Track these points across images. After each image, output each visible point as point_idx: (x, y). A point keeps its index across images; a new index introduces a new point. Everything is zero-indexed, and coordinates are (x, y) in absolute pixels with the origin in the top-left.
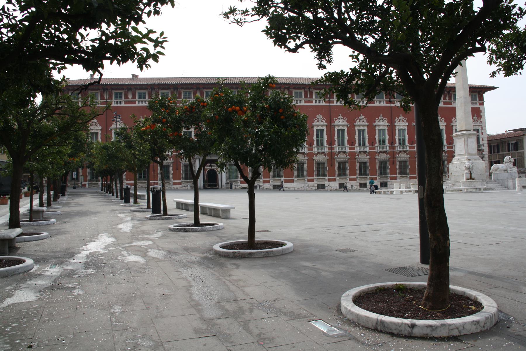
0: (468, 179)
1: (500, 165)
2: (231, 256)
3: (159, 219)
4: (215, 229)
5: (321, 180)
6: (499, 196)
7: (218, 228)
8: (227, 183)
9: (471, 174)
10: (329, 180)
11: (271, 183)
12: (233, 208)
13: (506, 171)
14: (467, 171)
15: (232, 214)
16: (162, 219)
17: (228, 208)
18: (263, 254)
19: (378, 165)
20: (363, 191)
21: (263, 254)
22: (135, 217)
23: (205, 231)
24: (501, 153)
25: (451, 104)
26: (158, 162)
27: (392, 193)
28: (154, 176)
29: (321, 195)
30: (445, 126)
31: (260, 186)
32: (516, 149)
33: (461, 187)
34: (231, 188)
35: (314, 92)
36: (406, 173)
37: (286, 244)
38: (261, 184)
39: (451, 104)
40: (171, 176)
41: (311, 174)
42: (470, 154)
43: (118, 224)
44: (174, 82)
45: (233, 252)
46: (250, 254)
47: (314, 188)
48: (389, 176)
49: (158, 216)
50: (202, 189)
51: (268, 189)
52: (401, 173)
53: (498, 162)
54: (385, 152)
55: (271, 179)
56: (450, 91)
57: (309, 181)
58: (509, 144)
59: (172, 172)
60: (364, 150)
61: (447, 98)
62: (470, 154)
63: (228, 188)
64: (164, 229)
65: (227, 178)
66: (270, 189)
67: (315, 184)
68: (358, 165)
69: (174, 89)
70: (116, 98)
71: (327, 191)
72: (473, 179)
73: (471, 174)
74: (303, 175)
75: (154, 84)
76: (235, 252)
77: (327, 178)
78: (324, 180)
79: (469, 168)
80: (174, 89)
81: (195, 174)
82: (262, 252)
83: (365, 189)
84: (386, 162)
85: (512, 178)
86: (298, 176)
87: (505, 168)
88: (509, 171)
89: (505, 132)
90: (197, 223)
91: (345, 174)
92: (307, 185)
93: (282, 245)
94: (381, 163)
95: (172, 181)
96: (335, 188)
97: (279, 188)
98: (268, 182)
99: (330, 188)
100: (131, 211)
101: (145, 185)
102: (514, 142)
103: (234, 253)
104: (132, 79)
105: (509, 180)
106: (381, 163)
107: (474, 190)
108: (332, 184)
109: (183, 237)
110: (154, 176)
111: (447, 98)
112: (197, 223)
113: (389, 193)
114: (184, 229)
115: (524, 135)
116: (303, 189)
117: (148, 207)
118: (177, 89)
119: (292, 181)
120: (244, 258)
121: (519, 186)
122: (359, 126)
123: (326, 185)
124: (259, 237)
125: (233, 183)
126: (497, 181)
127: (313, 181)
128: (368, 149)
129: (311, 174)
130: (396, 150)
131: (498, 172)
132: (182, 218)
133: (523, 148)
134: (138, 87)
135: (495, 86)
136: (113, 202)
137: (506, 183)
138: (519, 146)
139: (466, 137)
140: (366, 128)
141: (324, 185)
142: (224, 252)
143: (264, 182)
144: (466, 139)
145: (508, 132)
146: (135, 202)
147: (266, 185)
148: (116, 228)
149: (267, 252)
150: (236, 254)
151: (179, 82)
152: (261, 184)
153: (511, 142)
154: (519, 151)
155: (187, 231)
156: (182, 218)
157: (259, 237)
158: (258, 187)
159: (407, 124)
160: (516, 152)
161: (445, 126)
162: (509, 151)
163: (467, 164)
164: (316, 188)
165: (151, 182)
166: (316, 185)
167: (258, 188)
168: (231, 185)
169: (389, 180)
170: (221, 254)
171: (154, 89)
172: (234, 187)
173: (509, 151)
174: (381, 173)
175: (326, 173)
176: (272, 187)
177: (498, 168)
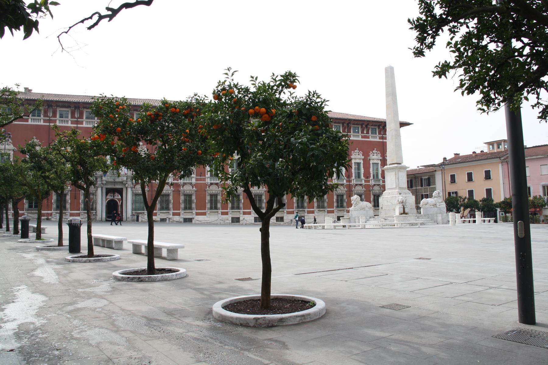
0: (401, 214)
1: (429, 200)
2: (252, 325)
3: (85, 262)
4: (178, 277)
5: (235, 213)
6: (432, 231)
7: (182, 276)
8: (133, 215)
9: (404, 208)
10: (244, 213)
11: (182, 216)
12: (183, 247)
13: (435, 205)
14: (401, 205)
15: (181, 254)
16: (90, 261)
17: (176, 247)
18: (298, 319)
19: (182, 198)
20: (280, 225)
21: (298, 319)
22: (49, 258)
23: (166, 280)
24: (414, 188)
25: (369, 138)
26: (83, 188)
27: (323, 228)
28: (48, 205)
29: (235, 230)
30: (363, 159)
31: (169, 219)
32: (429, 185)
33: (395, 222)
34: (138, 220)
35: (58, 110)
36: (323, 207)
37: (314, 305)
38: (171, 216)
39: (369, 138)
40: (68, 206)
41: (177, 207)
42: (400, 188)
43: (33, 270)
44: (75, 100)
45: (255, 318)
46: (281, 320)
47: (228, 221)
48: (306, 210)
49: (78, 257)
50: (101, 221)
51: (178, 222)
52: (318, 207)
53: (427, 196)
54: (361, 185)
55: (182, 212)
56: (368, 124)
57: (223, 214)
58: (421, 179)
59: (69, 201)
60: (378, 183)
61: (365, 132)
62: (400, 188)
63: (133, 221)
64: (107, 278)
65: (133, 209)
66: (181, 222)
67: (229, 217)
68: (208, 198)
69: (75, 108)
70: (61, 116)
71: (242, 224)
72: (406, 214)
73: (404, 208)
74: (216, 208)
75: (52, 101)
76: (259, 319)
77: (242, 211)
78: (238, 213)
79: (403, 202)
80: (75, 108)
81: (150, 205)
82: (297, 316)
83: (282, 223)
84: (261, 195)
85: (440, 213)
86: (211, 208)
87: (434, 202)
88: (438, 206)
89: (416, 168)
90: (151, 269)
91: (238, 208)
92: (220, 218)
93: (305, 304)
94: (211, 195)
95: (69, 212)
96: (251, 222)
97: (188, 221)
98: (179, 214)
99: (244, 222)
100: (38, 250)
101: (36, 216)
102: (427, 177)
103: (256, 319)
104: (25, 93)
105: (438, 215)
106: (211, 195)
107: (408, 225)
108: (247, 217)
109: (143, 290)
110: (48, 205)
111: (365, 132)
112: (151, 269)
113: (321, 228)
114: (134, 276)
115: (435, 171)
116: (215, 222)
117: (60, 244)
118: (79, 108)
119: (204, 214)
120: (273, 326)
121: (452, 221)
122: (355, 159)
123: (241, 219)
124: (274, 292)
125: (140, 215)
126: (427, 215)
127: (227, 214)
128: (363, 182)
129: (177, 207)
130: (352, 183)
131: (427, 206)
132: (115, 259)
133: (435, 184)
134: (61, 104)
135: (410, 122)
136: (4, 236)
137: (435, 218)
138: (431, 181)
139: (397, 171)
140: (362, 162)
141: (239, 218)
142: (240, 319)
143: (174, 214)
144: (397, 173)
145: (420, 167)
146: (39, 237)
147: (176, 218)
148: (33, 276)
149: (303, 316)
150: (259, 321)
151: (81, 100)
152: (171, 216)
153: (423, 178)
154: (431, 186)
155: (142, 281)
156: (115, 259)
157: (274, 292)
158: (168, 219)
159: (363, 157)
160: (428, 187)
161: (363, 159)
162: (422, 186)
163: (400, 198)
164: (231, 221)
165: (43, 212)
166: (230, 219)
167: (168, 221)
168: (138, 217)
169: (306, 214)
170: (234, 321)
171: (52, 106)
172: (140, 219)
173: (422, 186)
174: (298, 207)
175: (241, 205)
176: (182, 220)
177: (428, 203)
